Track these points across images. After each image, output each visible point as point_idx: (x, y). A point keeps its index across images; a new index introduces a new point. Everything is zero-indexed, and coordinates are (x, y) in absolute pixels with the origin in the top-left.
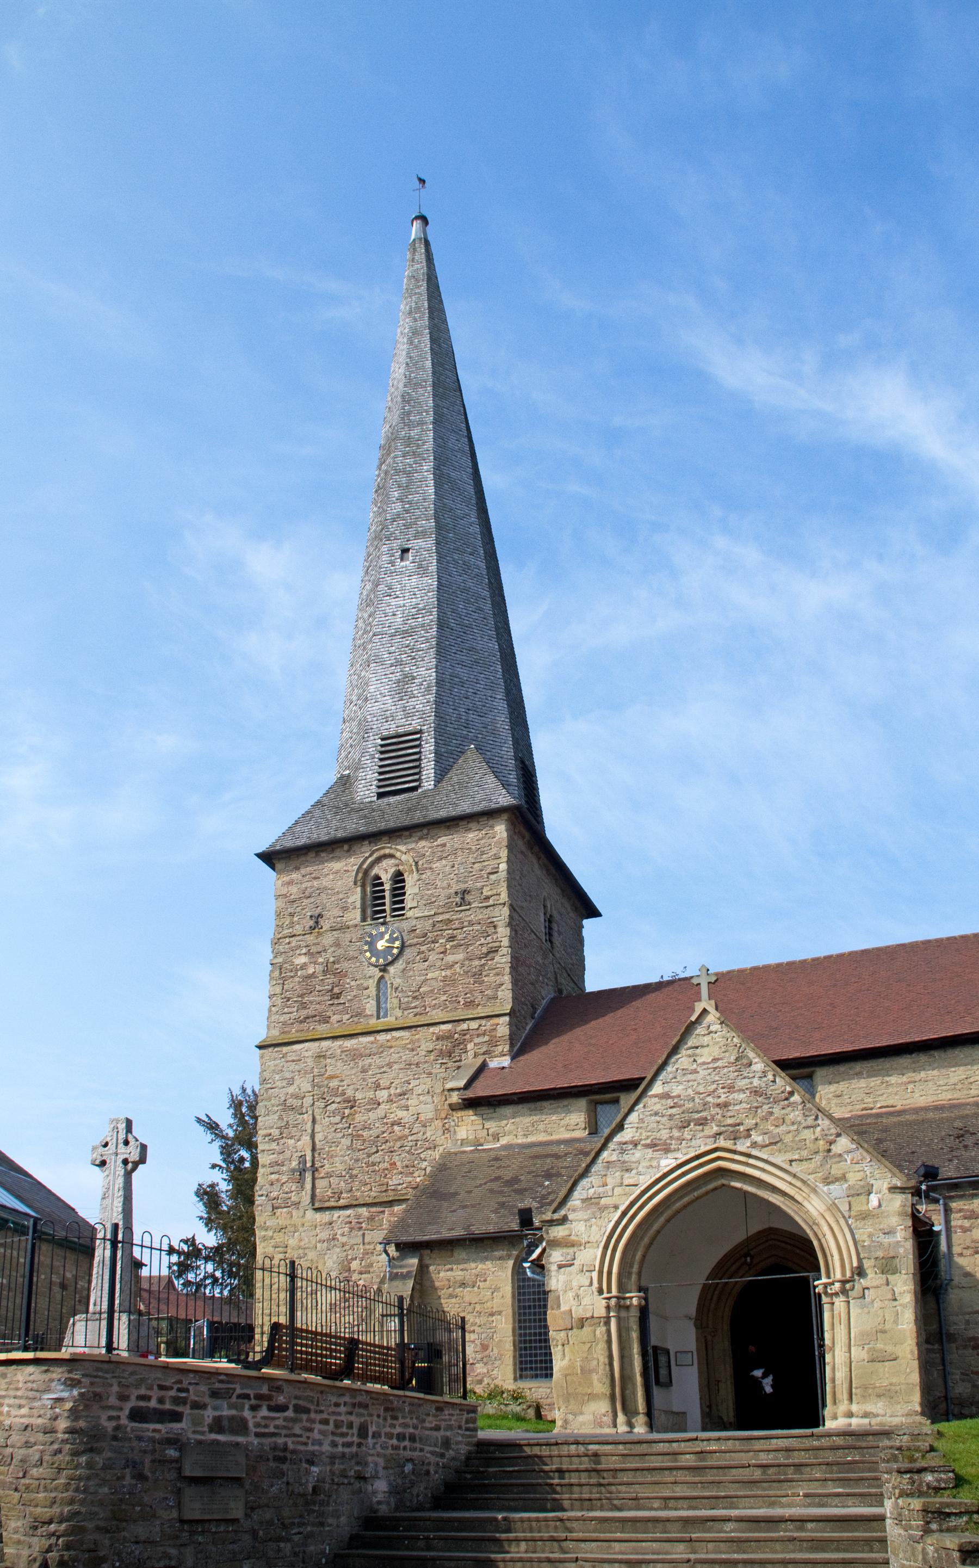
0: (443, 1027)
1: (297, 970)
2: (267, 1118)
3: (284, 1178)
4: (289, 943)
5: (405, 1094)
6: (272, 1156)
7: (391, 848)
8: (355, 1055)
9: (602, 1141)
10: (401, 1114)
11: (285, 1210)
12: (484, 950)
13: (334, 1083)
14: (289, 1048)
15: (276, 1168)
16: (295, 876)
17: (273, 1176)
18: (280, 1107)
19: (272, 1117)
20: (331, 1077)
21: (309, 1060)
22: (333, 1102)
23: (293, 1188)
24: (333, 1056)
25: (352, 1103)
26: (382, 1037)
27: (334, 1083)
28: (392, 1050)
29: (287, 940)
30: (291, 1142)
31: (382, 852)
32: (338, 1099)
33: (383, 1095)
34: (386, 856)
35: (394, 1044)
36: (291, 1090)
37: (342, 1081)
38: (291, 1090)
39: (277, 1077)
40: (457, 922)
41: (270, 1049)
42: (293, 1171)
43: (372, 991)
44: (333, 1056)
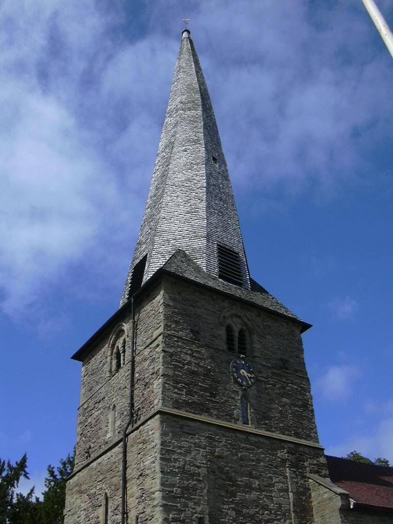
1: (184, 365)
22: (219, 478)
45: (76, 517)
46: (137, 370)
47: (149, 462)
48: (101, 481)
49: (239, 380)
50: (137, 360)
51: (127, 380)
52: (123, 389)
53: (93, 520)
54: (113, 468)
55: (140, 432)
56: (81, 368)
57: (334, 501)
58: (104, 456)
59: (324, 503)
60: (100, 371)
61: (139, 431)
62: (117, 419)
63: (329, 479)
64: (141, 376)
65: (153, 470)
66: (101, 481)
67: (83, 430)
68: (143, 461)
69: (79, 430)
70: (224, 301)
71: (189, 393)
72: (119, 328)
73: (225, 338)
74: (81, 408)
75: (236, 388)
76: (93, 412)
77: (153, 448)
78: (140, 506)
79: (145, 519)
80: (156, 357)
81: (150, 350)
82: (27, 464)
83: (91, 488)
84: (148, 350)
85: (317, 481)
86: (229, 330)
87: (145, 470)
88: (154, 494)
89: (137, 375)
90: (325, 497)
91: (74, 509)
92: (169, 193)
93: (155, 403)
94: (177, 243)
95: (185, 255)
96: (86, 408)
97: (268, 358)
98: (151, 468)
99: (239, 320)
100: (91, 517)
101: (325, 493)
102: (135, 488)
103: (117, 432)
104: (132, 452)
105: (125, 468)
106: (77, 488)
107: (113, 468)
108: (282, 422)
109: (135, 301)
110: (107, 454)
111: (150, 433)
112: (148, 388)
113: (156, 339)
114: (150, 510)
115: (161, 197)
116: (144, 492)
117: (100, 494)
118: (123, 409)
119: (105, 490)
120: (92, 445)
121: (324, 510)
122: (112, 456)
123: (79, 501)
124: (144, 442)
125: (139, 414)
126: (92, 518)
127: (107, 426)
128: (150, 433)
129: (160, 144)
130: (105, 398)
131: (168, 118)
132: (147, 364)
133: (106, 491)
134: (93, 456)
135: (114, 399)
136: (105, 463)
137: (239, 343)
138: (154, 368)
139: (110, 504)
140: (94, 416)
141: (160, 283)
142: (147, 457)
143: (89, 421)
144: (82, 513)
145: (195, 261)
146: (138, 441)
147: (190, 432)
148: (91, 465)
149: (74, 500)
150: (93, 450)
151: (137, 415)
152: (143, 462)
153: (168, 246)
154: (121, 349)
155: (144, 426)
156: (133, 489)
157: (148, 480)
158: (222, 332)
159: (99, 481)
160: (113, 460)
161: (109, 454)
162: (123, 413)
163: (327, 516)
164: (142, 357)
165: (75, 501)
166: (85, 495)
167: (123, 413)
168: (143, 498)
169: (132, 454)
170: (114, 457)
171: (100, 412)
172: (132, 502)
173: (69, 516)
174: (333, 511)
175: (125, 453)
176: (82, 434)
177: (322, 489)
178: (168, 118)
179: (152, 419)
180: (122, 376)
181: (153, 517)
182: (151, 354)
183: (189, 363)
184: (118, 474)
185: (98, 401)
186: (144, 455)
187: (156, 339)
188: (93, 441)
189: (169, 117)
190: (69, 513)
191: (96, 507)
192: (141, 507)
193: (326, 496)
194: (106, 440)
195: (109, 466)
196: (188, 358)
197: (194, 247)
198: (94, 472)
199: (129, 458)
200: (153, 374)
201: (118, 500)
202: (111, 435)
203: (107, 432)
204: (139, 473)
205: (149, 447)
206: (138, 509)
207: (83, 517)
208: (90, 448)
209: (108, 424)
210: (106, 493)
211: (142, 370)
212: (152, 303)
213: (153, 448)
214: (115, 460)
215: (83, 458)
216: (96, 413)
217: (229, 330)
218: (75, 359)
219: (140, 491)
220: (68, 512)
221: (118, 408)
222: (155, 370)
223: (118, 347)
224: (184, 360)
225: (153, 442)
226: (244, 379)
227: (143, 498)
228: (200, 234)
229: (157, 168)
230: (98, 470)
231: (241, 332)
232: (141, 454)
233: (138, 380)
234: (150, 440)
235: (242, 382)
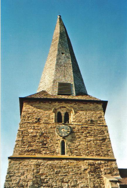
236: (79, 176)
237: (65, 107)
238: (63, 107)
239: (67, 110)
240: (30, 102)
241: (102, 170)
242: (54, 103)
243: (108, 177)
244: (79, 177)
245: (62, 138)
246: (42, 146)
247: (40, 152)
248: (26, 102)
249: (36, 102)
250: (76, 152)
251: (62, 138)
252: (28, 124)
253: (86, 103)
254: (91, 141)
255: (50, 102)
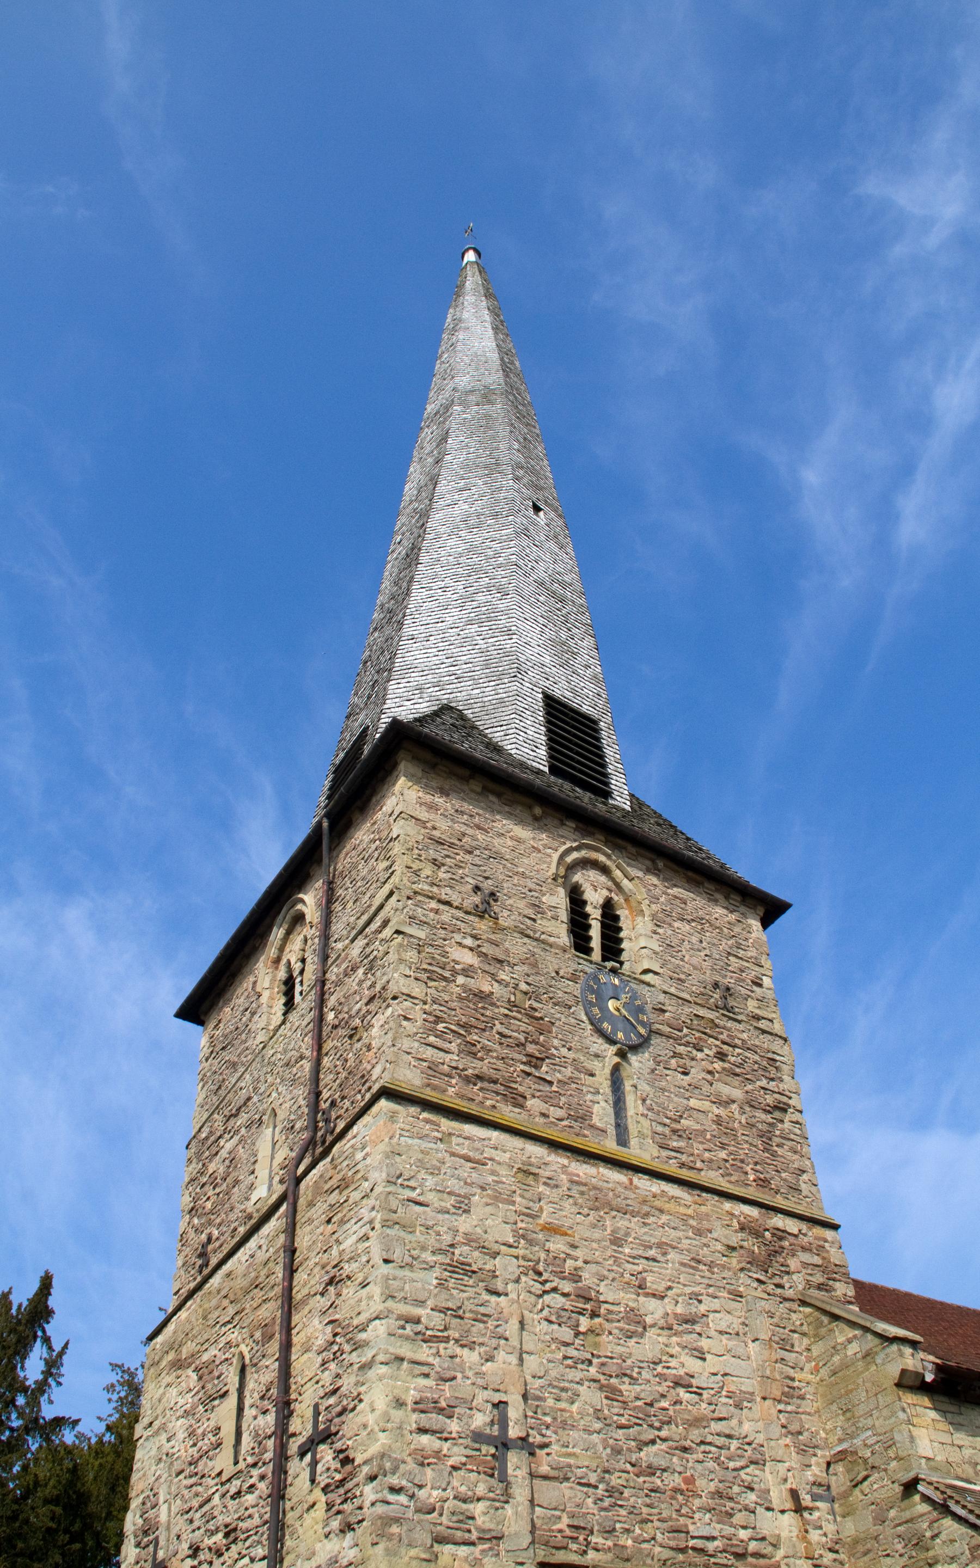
0: (747, 1209)
1: (455, 972)
2: (407, 1273)
3: (457, 1454)
4: (437, 912)
5: (694, 1322)
6: (423, 1382)
7: (608, 856)
8: (600, 1202)
9: (231, 1451)
10: (693, 1365)
11: (463, 1551)
12: (770, 1099)
13: (557, 1245)
14: (455, 1124)
15: (434, 1420)
16: (439, 800)
17: (425, 1439)
18: (439, 1258)
19: (420, 1275)
20: (552, 1230)
21: (503, 1171)
22: (555, 1290)
23: (481, 1490)
24: (551, 1183)
25: (588, 1302)
26: (643, 1183)
27: (557, 1245)
28: (664, 1218)
29: (433, 905)
30: (471, 1357)
31: (594, 855)
32: (567, 1287)
33: (654, 1310)
34: (595, 865)
35: (667, 1206)
36: (465, 1224)
37: (574, 1247)
38: (465, 1224)
39: (430, 1182)
40: (726, 1033)
41: (413, 1110)
42: (478, 1437)
43: (606, 1087)
44: (551, 1183)
45: (164, 1437)
46: (332, 1001)
47: (354, 1238)
48: (229, 1322)
49: (605, 1025)
50: (334, 978)
51: (306, 1035)
52: (297, 1062)
53: (206, 1441)
54: (260, 1280)
55: (333, 1160)
56: (199, 1038)
57: (879, 1361)
58: (242, 1249)
59: (848, 1372)
60: (244, 1035)
61: (329, 1159)
62: (277, 1146)
63: (856, 1308)
64: (340, 1017)
65: (364, 1259)
66: (229, 1322)
67: (195, 1200)
68: (337, 1241)
69: (186, 1200)
70: (563, 824)
71: (470, 1050)
72: (292, 912)
73: (564, 916)
74: (193, 1143)
75: (599, 1045)
76: (222, 1144)
77: (366, 1196)
78: (327, 1372)
79: (339, 1409)
80: (380, 955)
81: (366, 941)
82: (52, 1302)
83: (205, 1347)
84: (361, 942)
85: (828, 1308)
86: (576, 901)
87: (342, 1264)
88: (364, 1330)
89: (331, 1016)
90: (850, 1353)
91: (160, 1418)
92: (424, 581)
93: (374, 1078)
94: (443, 692)
95: (462, 717)
96: (207, 1138)
97: (679, 979)
98: (359, 1255)
99: (603, 879)
100: (200, 1431)
101: (850, 1341)
102: (316, 1321)
103: (277, 1179)
104: (310, 1221)
105: (291, 1270)
106: (171, 1356)
107: (260, 1280)
108: (723, 1146)
109: (331, 827)
110: (248, 1245)
111: (359, 1156)
112: (359, 1040)
113: (381, 907)
114: (353, 1379)
115: (408, 593)
116: (339, 1330)
117: (227, 1359)
118: (292, 1117)
119: (238, 1346)
120: (216, 1233)
121: (851, 1391)
122: (260, 1247)
123: (173, 1391)
124: (343, 1185)
125: (334, 1117)
126: (204, 1435)
127: (253, 1172)
128: (359, 1156)
129: (407, 487)
130: (249, 1099)
131: (426, 430)
132: (357, 980)
133: (243, 1348)
134: (214, 1261)
135: (274, 1095)
136: (241, 1269)
137: (604, 936)
138: (373, 985)
139: (251, 1385)
140: (223, 1153)
141: (395, 766)
142: (348, 1225)
143: (211, 1171)
144: (179, 1423)
145: (487, 731)
146: (326, 1187)
147: (471, 1154)
148: (208, 1286)
149: (161, 1391)
150: (217, 1244)
151: (327, 1121)
152: (338, 1242)
153: (421, 701)
154: (297, 967)
155: (344, 1141)
156: (311, 1329)
157: (348, 1291)
158: (559, 899)
159: (224, 1325)
160: (261, 1256)
161: (252, 1244)
162: (292, 1127)
163: (861, 1410)
164: (344, 966)
165: (164, 1393)
166: (189, 1371)
167: (292, 1127)
168: (336, 1348)
169: (309, 1228)
170: (264, 1248)
171: (236, 1138)
172: (305, 1364)
173: (147, 1439)
174: (876, 1395)
175: (291, 1229)
176: (192, 1209)
177: (841, 1332)
178: (426, 430)
179: (366, 1117)
180: (294, 1028)
181: (361, 1401)
182: (368, 950)
183: (468, 971)
184: (271, 1294)
185: (234, 1111)
186: (342, 1222)
187: (381, 907)
188: (218, 1221)
189: (428, 427)
190: (149, 1432)
191: (212, 1399)
192: (327, 1377)
193: (853, 1349)
194: (249, 1210)
195: (253, 1275)
196: (468, 958)
197: (486, 699)
198: (214, 1302)
199: (303, 1240)
200: (372, 999)
201: (267, 1373)
202: (263, 1192)
203: (251, 1187)
204: (326, 1278)
205: (356, 1196)
206: (320, 1384)
207: (181, 1435)
208: (209, 1240)
209: (257, 1166)
210: (241, 1353)
211: (343, 1000)
212: (375, 823)
213: (366, 1196)
214: (268, 1255)
215: (192, 1272)
216: (229, 1146)
217: (576, 901)
218: (184, 1019)
219: (329, 1329)
220: (146, 1428)
221: (281, 1115)
222: (378, 987)
223: (289, 962)
224: (457, 963)
225: (366, 1180)
226: (620, 1025)
227: (336, 1348)
228: (500, 669)
229: (398, 540)
230: (223, 1293)
231: (608, 909)
232: (333, 1220)
233: (335, 1027)
234: (359, 1175)
235: (615, 1031)
236: (707, 1274)
237: (605, 870)
238: (595, 865)
239: (610, 891)
240: (433, 766)
241: (793, 1264)
242: (556, 822)
243: (383, 1444)
244: (706, 1281)
245: (613, 1049)
246: (527, 1069)
247: (518, 1100)
248: (416, 759)
249: (465, 780)
250: (675, 1144)
251: (613, 1049)
252: (442, 907)
253: (698, 878)
254: (734, 1102)
255: (538, 811)
